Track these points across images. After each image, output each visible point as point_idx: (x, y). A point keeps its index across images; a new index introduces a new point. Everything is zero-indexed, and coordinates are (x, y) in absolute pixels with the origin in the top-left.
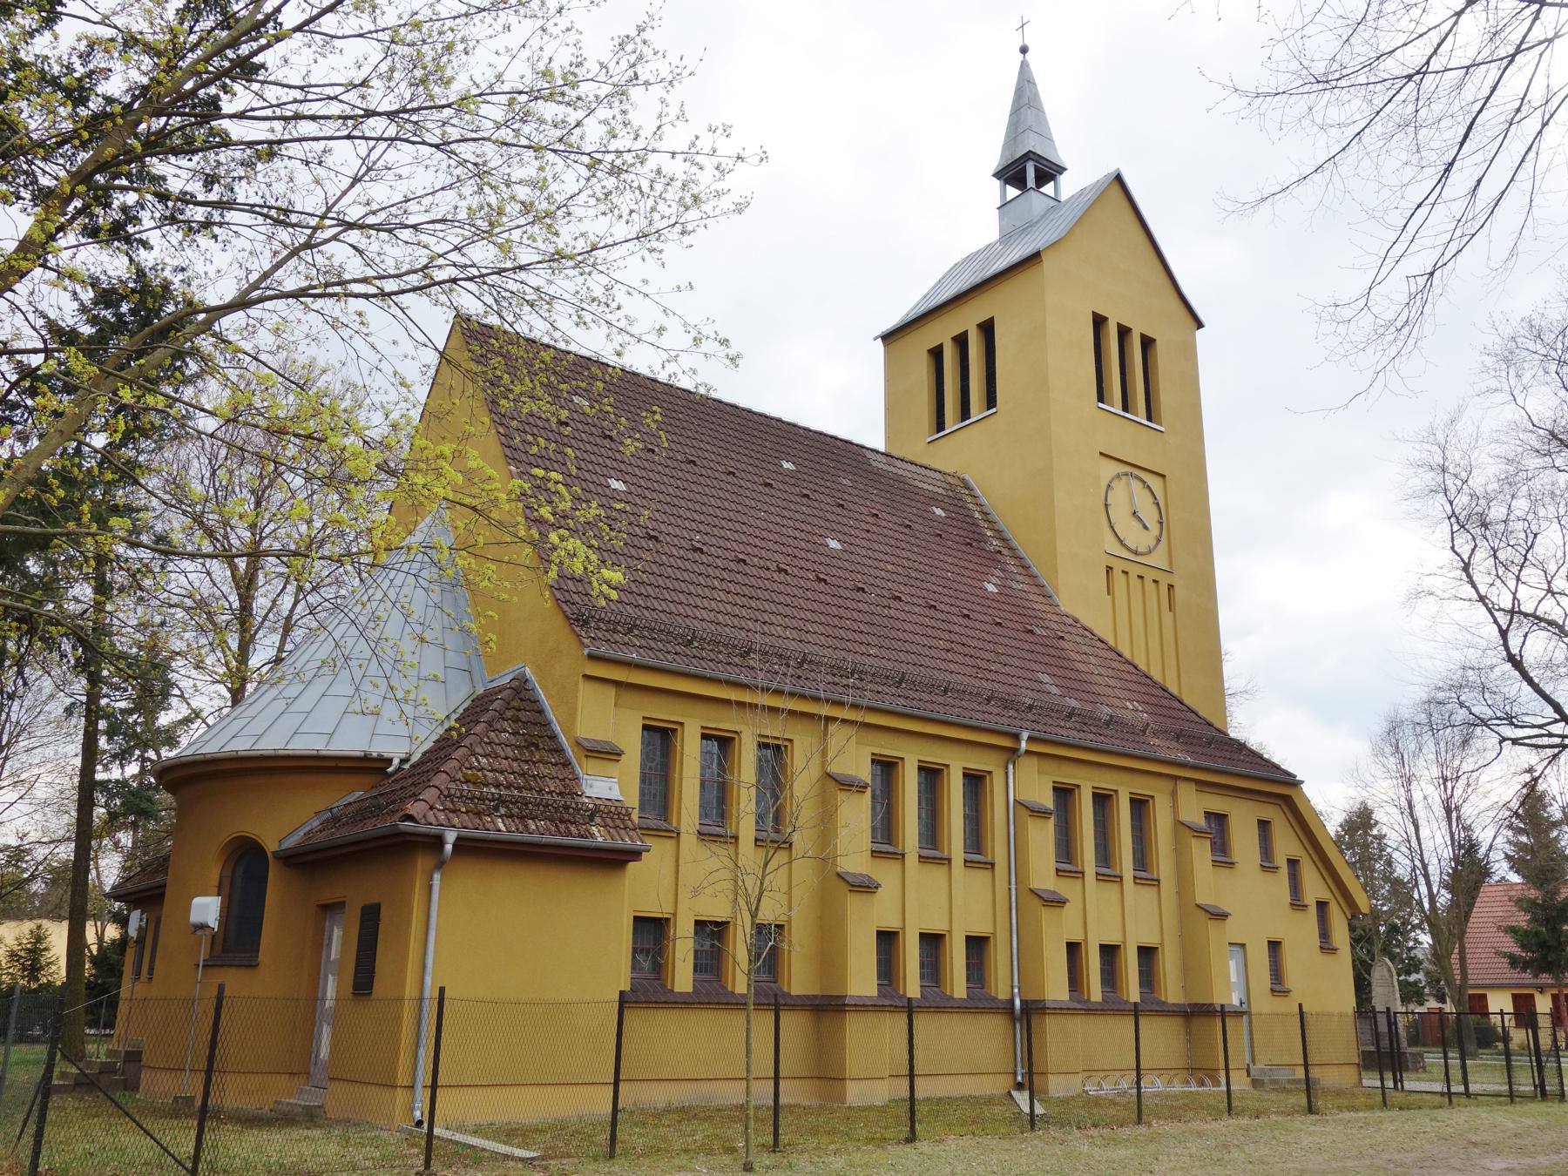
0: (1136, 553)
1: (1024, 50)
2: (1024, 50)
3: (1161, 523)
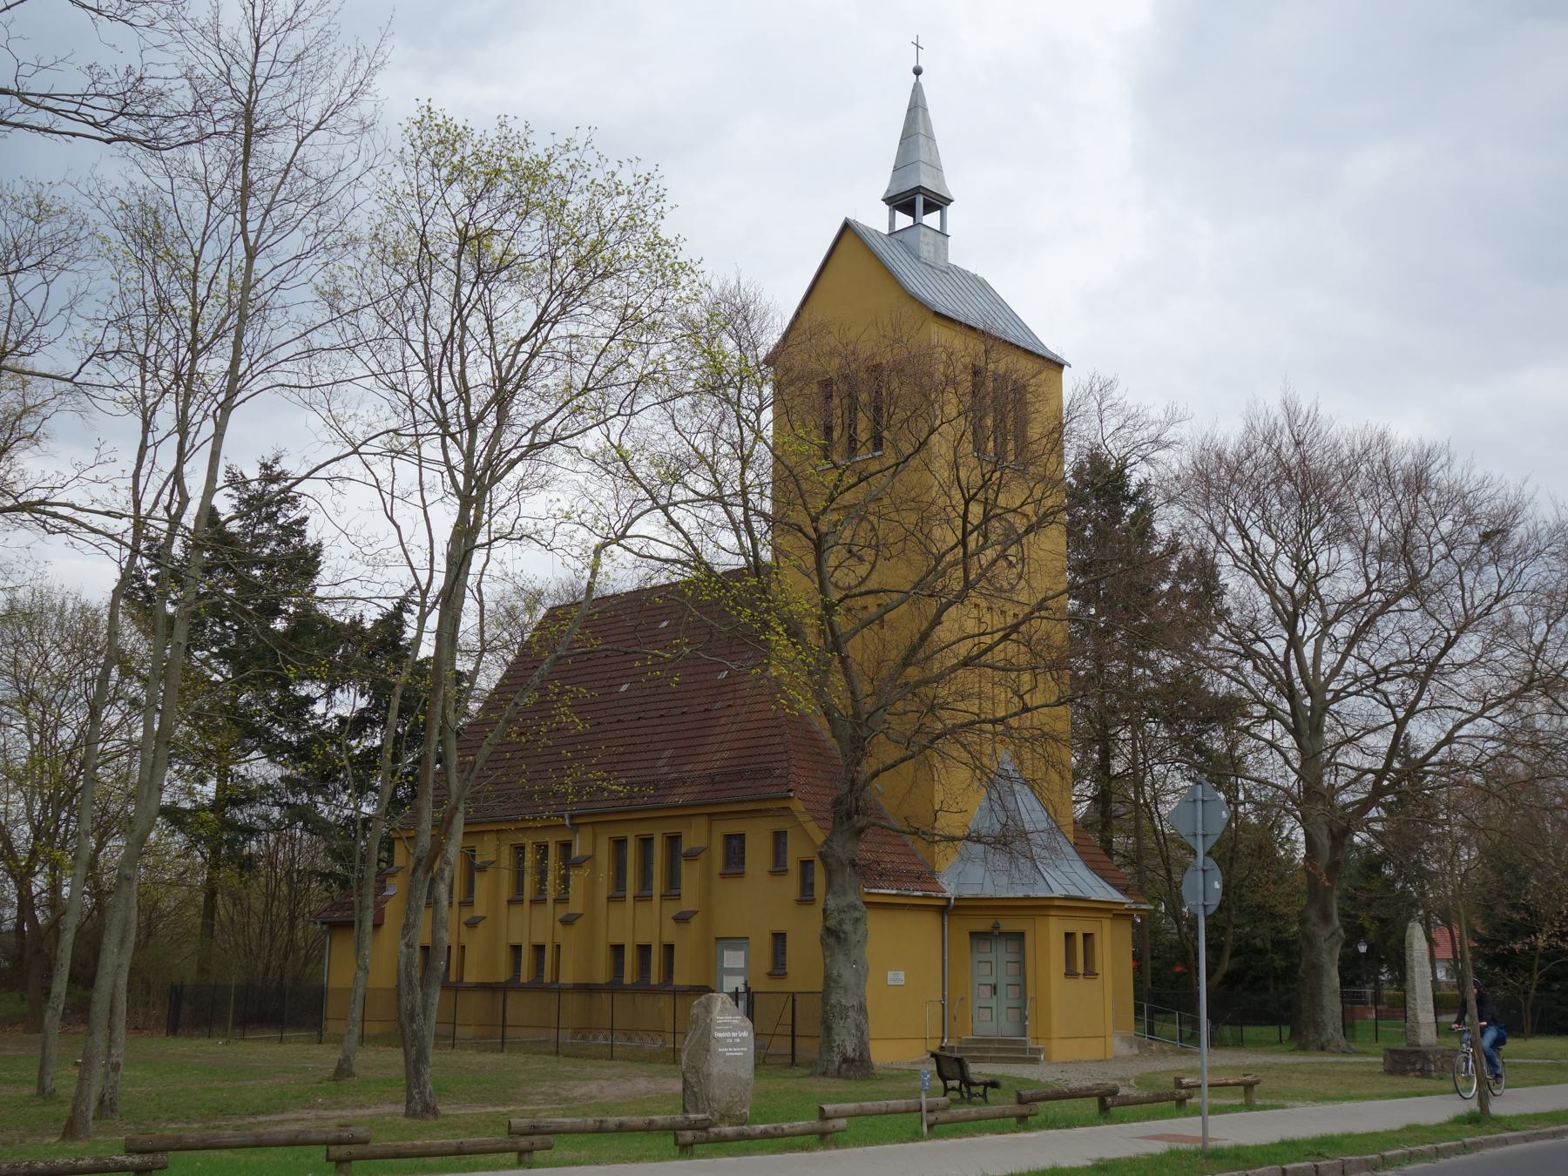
1: (918, 72)
2: (918, 72)
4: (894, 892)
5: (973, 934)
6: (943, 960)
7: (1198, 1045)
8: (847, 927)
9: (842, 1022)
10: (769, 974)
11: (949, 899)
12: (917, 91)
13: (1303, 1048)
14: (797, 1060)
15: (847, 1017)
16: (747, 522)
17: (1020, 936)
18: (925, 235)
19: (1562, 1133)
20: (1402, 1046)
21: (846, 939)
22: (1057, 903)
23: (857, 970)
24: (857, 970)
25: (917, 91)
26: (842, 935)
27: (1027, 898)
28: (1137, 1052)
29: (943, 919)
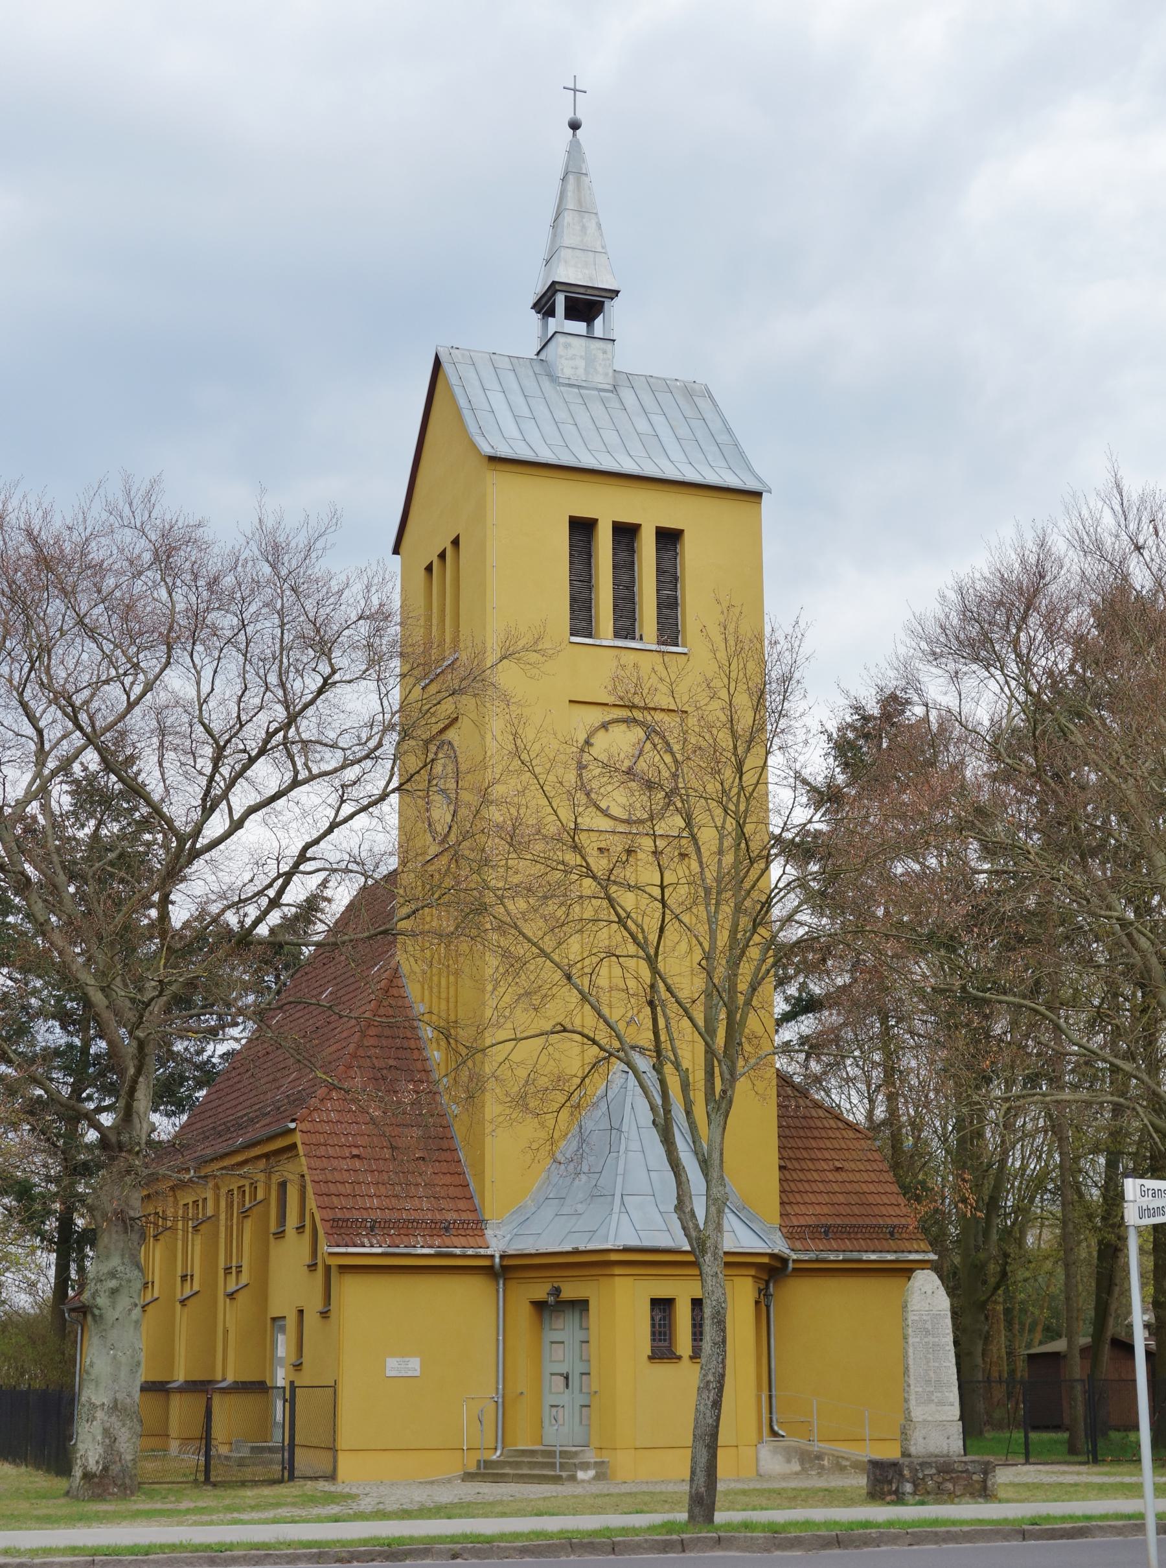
1: (575, 126)
2: (575, 126)
4: (379, 1250)
5: (540, 1306)
6: (498, 1340)
7: (1135, 1459)
8: (102, 1301)
9: (87, 1425)
10: (650, 1358)
11: (492, 1256)
12: (575, 150)
13: (1095, 1458)
14: (296, 1474)
15: (94, 1418)
16: (1007, 682)
17: (582, 1305)
18: (567, 346)
19: (6, 1552)
20: (890, 1452)
21: (101, 1316)
22: (614, 1257)
23: (115, 1357)
24: (115, 1357)
25: (575, 150)
26: (97, 1312)
27: (576, 1252)
28: (797, 1467)
29: (498, 1285)
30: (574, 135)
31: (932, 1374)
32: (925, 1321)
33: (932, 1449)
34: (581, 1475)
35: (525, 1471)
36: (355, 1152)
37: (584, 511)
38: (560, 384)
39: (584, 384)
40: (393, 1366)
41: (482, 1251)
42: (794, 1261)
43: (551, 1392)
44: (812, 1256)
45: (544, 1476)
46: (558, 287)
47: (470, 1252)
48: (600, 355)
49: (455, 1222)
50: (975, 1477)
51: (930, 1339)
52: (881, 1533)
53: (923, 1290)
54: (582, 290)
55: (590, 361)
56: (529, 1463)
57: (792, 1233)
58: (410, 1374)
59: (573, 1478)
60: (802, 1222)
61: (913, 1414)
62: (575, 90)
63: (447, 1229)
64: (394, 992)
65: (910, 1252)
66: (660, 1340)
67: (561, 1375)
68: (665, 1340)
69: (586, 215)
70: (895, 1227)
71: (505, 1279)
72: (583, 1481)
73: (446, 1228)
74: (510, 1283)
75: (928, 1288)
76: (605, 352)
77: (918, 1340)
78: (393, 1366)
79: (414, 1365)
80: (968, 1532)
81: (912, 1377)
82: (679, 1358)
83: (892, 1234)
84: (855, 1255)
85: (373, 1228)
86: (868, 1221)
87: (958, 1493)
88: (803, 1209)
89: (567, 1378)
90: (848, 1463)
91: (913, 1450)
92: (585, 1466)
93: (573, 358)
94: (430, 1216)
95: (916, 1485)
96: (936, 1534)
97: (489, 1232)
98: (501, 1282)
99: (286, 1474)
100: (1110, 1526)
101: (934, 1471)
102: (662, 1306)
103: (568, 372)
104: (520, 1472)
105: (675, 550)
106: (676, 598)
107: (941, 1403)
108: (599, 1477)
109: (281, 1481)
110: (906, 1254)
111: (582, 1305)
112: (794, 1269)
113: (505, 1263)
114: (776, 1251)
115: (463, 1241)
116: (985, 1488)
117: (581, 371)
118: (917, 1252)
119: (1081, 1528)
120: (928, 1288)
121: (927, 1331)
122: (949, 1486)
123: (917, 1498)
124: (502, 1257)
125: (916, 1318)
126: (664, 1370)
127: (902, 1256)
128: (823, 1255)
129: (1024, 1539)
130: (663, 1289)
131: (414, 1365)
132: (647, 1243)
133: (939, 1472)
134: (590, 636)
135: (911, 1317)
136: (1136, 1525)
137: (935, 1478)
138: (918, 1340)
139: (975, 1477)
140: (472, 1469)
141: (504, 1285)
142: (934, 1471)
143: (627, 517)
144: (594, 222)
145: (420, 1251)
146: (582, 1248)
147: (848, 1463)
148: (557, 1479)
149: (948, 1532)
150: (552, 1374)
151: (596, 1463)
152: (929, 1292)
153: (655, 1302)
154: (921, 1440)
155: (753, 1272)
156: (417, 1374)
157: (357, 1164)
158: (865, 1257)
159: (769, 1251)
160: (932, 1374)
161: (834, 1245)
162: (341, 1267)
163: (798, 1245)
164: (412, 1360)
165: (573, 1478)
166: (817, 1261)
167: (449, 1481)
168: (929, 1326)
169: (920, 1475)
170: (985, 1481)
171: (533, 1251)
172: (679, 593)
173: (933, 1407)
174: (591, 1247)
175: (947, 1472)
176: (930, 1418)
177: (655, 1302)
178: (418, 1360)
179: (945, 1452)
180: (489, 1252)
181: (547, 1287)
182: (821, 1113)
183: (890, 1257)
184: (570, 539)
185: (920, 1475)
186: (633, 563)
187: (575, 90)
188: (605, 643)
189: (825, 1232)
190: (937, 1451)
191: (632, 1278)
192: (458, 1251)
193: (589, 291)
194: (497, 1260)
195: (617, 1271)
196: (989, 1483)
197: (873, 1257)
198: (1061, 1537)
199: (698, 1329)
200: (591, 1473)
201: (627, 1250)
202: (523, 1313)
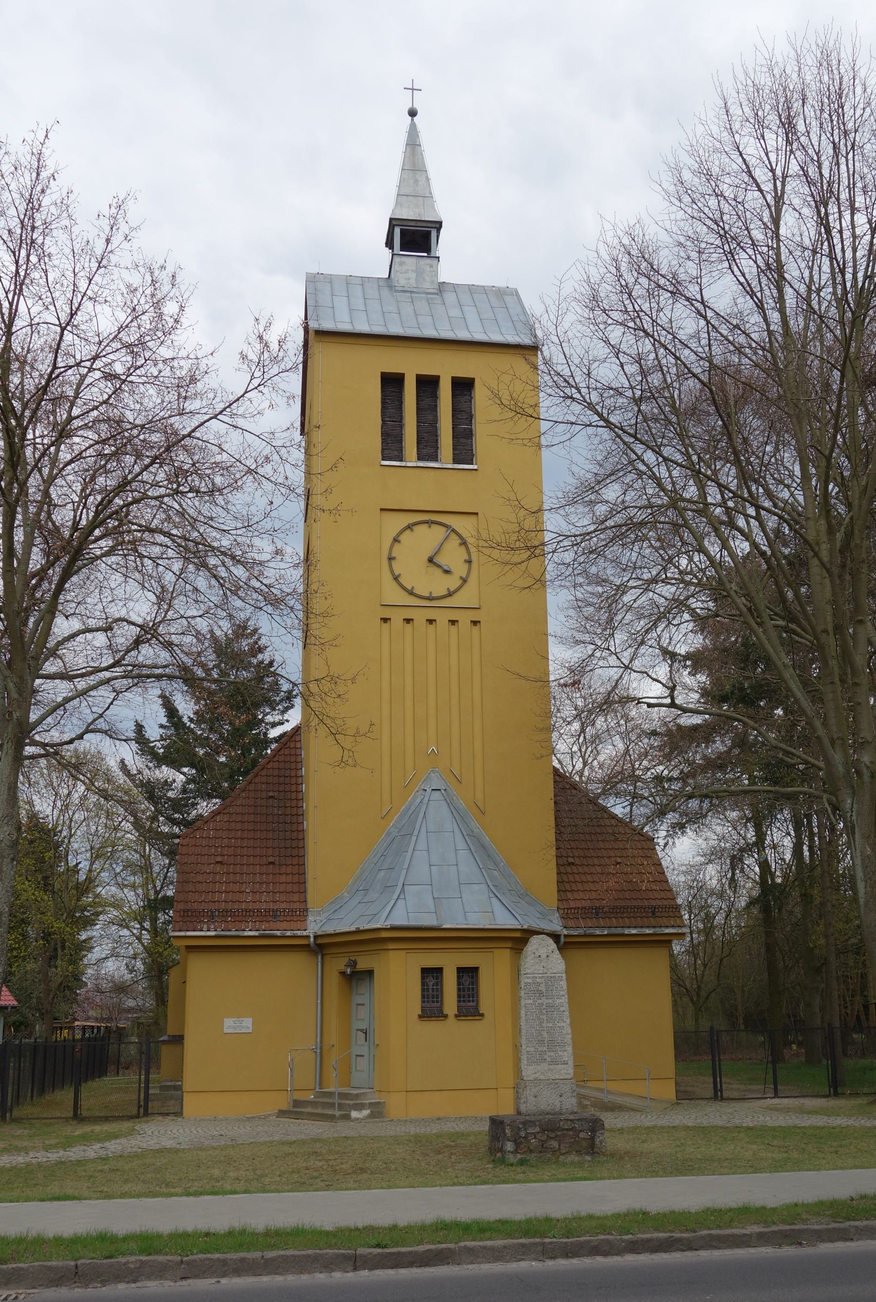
0: (430, 598)
1: (413, 113)
2: (413, 113)
3: (469, 562)
10: (420, 1017)
11: (308, 937)
12: (413, 132)
17: (370, 973)
25: (413, 132)
27: (358, 932)
30: (412, 120)
31: (545, 1035)
32: (539, 984)
33: (543, 1106)
34: (354, 1114)
35: (319, 1111)
36: (219, 859)
37: (393, 368)
38: (396, 291)
39: (415, 290)
40: (229, 1025)
41: (299, 933)
42: (565, 936)
43: (356, 1044)
44: (581, 931)
45: (326, 1115)
46: (394, 223)
47: (289, 933)
48: (428, 269)
49: (284, 911)
50: (582, 1135)
51: (544, 1001)
52: (142, 1262)
53: (537, 954)
54: (413, 224)
55: (419, 273)
56: (323, 1103)
57: (566, 915)
58: (244, 1031)
59: (347, 1117)
60: (579, 904)
61: (524, 1074)
62: (413, 89)
63: (275, 916)
64: (292, 745)
65: (667, 927)
66: (433, 1002)
67: (361, 1030)
68: (437, 1002)
69: (419, 173)
70: (655, 908)
71: (323, 955)
72: (357, 1119)
73: (273, 915)
74: (327, 958)
75: (543, 952)
76: (431, 266)
77: (531, 1002)
78: (229, 1025)
79: (247, 1024)
80: (273, 1259)
81: (524, 1038)
82: (446, 1016)
83: (653, 913)
84: (619, 931)
85: (211, 917)
86: (635, 903)
87: (564, 1151)
88: (582, 895)
89: (366, 1033)
90: (588, 1103)
91: (523, 1108)
92: (359, 1107)
93: (407, 272)
94: (264, 907)
95: (517, 1144)
96: (224, 1262)
97: (311, 918)
98: (320, 957)
99: (142, 1110)
100: (484, 1248)
101: (538, 1129)
102: (432, 975)
103: (403, 282)
104: (316, 1111)
105: (470, 395)
106: (471, 430)
107: (554, 1062)
108: (372, 1116)
109: (138, 1116)
110: (663, 929)
111: (370, 973)
112: (565, 943)
113: (319, 941)
114: (525, 927)
115: (285, 925)
116: (592, 1145)
117: (413, 281)
118: (673, 926)
119: (441, 1251)
120: (543, 952)
121: (541, 993)
122: (555, 1144)
123: (519, 1156)
124: (316, 937)
125: (530, 981)
126: (433, 1027)
127: (658, 930)
128: (591, 931)
129: (355, 1269)
130: (432, 960)
131: (247, 1024)
132: (413, 923)
133: (543, 1130)
134: (401, 460)
135: (524, 980)
136: (523, 1245)
137: (539, 1136)
138: (531, 1002)
139: (582, 1135)
140: (284, 1107)
141: (322, 959)
142: (538, 1129)
143: (428, 371)
144: (424, 177)
145: (246, 934)
146: (362, 928)
147: (588, 1103)
148: (331, 1118)
149: (243, 1260)
150: (357, 1030)
151: (371, 1104)
152: (544, 956)
153: (425, 971)
154: (532, 1098)
155: (510, 945)
156: (250, 1030)
157: (218, 868)
158: (626, 931)
159: (519, 927)
160: (545, 1035)
161: (601, 921)
162: (187, 947)
163: (571, 923)
164: (245, 1019)
165: (347, 1117)
166: (585, 935)
167: (266, 1117)
168: (543, 988)
169: (523, 1134)
170: (592, 1139)
171: (332, 932)
172: (473, 427)
173: (544, 1066)
174: (367, 927)
175: (553, 1131)
176: (542, 1077)
177: (425, 971)
178: (226, 1020)
179: (557, 1109)
180: (305, 933)
181: (345, 961)
182: (613, 822)
183: (648, 931)
184: (382, 391)
185: (523, 1134)
186: (436, 406)
187: (413, 89)
188: (409, 464)
189: (595, 912)
190: (548, 1109)
191: (404, 952)
192: (278, 933)
193: (419, 224)
194: (312, 940)
195: (391, 946)
196: (597, 1141)
197: (634, 931)
198: (411, 1264)
199: (426, 993)
200: (366, 1112)
201: (394, 928)
202: (334, 981)
